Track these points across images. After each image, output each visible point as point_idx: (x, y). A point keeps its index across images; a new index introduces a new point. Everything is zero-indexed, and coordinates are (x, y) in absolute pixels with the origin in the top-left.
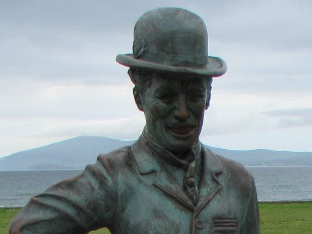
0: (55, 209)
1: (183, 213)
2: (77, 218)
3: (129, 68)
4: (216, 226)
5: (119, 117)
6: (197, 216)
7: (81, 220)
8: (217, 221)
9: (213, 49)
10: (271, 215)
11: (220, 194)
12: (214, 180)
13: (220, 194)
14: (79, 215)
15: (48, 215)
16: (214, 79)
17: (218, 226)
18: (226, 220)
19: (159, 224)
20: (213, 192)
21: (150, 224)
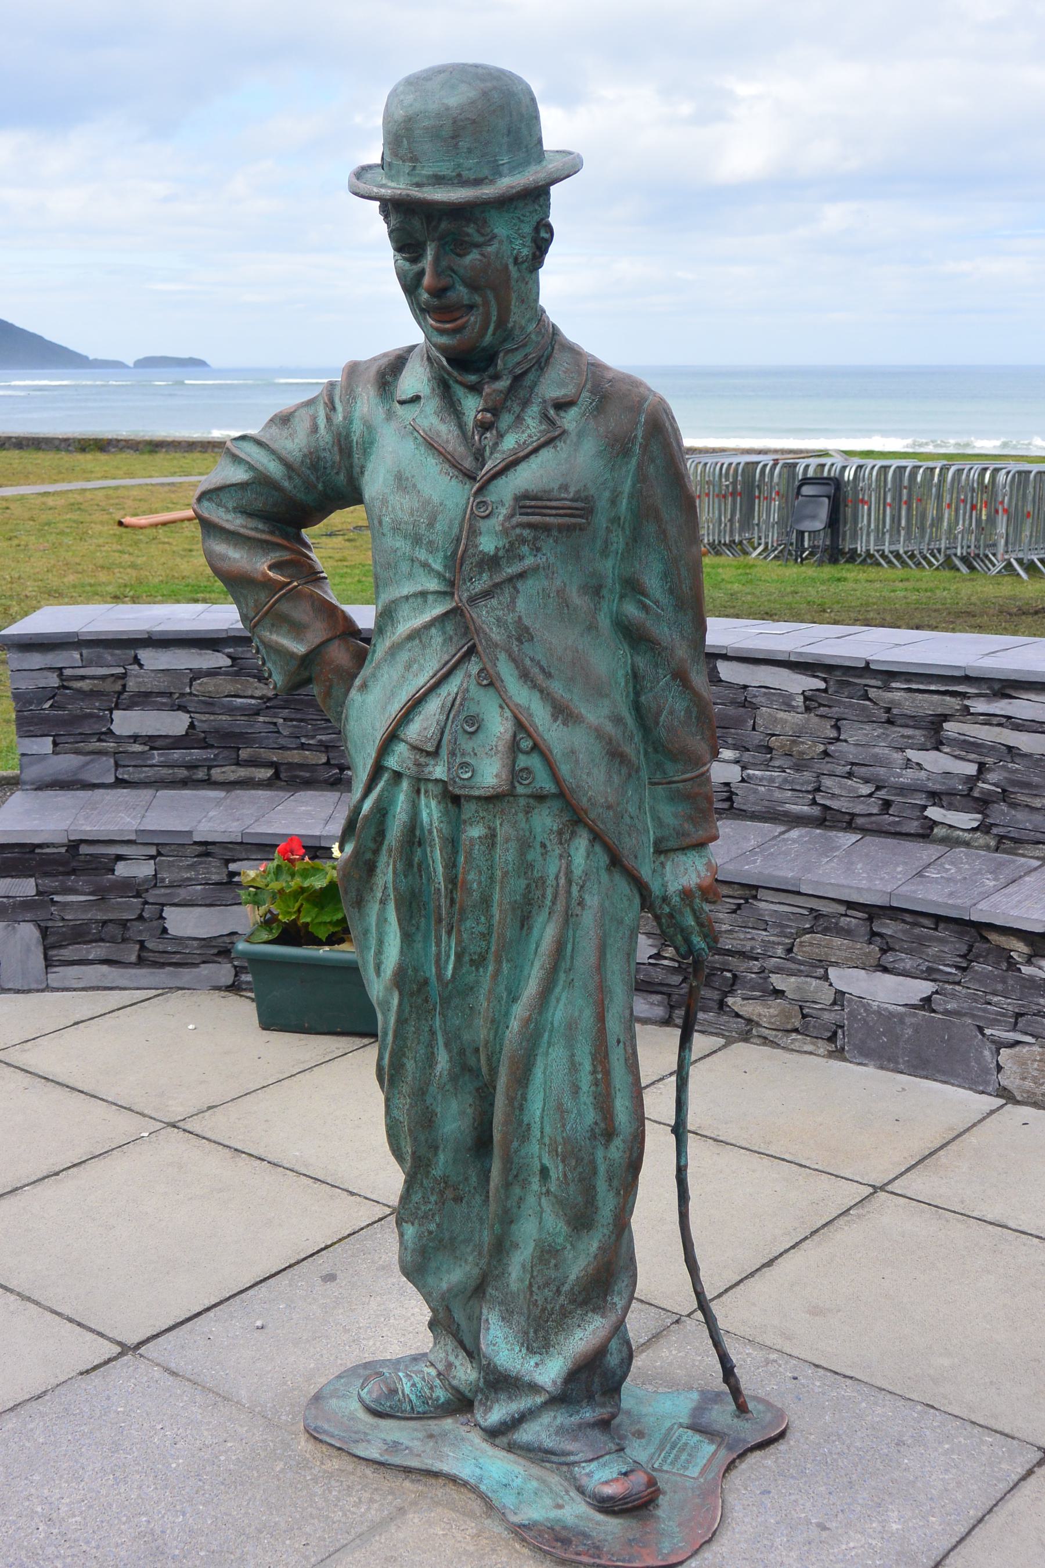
0: (251, 467)
1: (454, 482)
2: (286, 484)
3: (378, 203)
4: (521, 514)
5: (369, 308)
6: (480, 490)
7: (295, 487)
8: (528, 503)
9: (556, 130)
10: (763, 970)
11: (555, 447)
12: (545, 417)
13: (555, 447)
14: (290, 478)
15: (239, 475)
16: (553, 189)
17: (527, 514)
18: (549, 503)
19: (401, 504)
20: (533, 442)
21: (387, 502)
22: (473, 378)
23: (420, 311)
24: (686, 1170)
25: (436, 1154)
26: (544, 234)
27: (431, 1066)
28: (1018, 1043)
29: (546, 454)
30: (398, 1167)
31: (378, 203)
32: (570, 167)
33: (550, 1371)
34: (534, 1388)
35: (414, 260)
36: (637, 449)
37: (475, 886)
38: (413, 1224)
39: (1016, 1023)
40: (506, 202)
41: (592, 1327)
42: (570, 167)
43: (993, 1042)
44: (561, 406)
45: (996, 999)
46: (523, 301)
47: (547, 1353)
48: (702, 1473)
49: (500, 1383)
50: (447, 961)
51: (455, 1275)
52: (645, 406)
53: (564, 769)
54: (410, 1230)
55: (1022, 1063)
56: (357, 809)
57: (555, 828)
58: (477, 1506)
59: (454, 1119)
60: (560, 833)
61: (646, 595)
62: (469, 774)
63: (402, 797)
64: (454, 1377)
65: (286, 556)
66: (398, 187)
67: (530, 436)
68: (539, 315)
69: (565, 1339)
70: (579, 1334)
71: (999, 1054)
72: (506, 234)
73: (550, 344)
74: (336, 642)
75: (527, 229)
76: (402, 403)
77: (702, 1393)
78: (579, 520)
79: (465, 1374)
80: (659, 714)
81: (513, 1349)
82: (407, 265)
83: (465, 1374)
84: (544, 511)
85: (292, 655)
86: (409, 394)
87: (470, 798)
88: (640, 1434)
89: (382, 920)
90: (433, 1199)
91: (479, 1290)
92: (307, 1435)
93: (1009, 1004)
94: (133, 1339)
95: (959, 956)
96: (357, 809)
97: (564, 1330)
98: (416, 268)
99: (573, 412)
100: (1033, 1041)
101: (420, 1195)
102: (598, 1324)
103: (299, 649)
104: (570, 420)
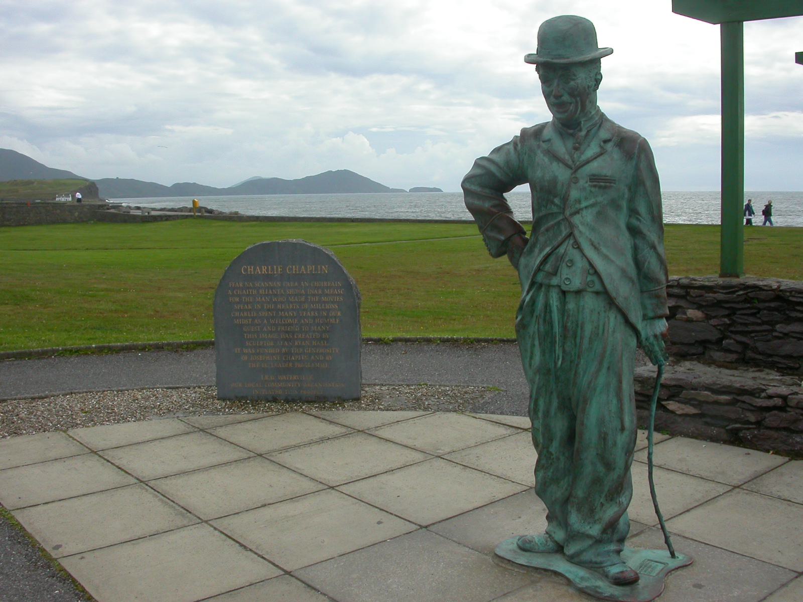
22: (571, 131)
23: (551, 105)
24: (652, 454)
25: (552, 443)
26: (599, 77)
29: (600, 160)
30: (535, 450)
31: (534, 66)
32: (609, 52)
33: (595, 530)
34: (589, 537)
35: (549, 86)
36: (635, 157)
40: (583, 64)
42: (609, 52)
44: (605, 142)
46: (590, 102)
48: (656, 575)
49: (573, 536)
50: (558, 359)
51: (558, 492)
52: (639, 141)
53: (607, 282)
54: (541, 474)
56: (524, 301)
58: (563, 581)
59: (559, 426)
61: (640, 215)
62: (570, 265)
65: (497, 202)
66: (541, 60)
68: (598, 110)
72: (581, 78)
73: (603, 118)
74: (516, 236)
75: (592, 75)
76: (544, 142)
77: (647, 438)
79: (560, 535)
80: (644, 263)
83: (560, 535)
85: (499, 240)
86: (547, 138)
87: (569, 292)
88: (617, 214)
89: (533, 345)
91: (566, 501)
94: (424, 524)
96: (524, 301)
103: (503, 238)
104: (609, 146)
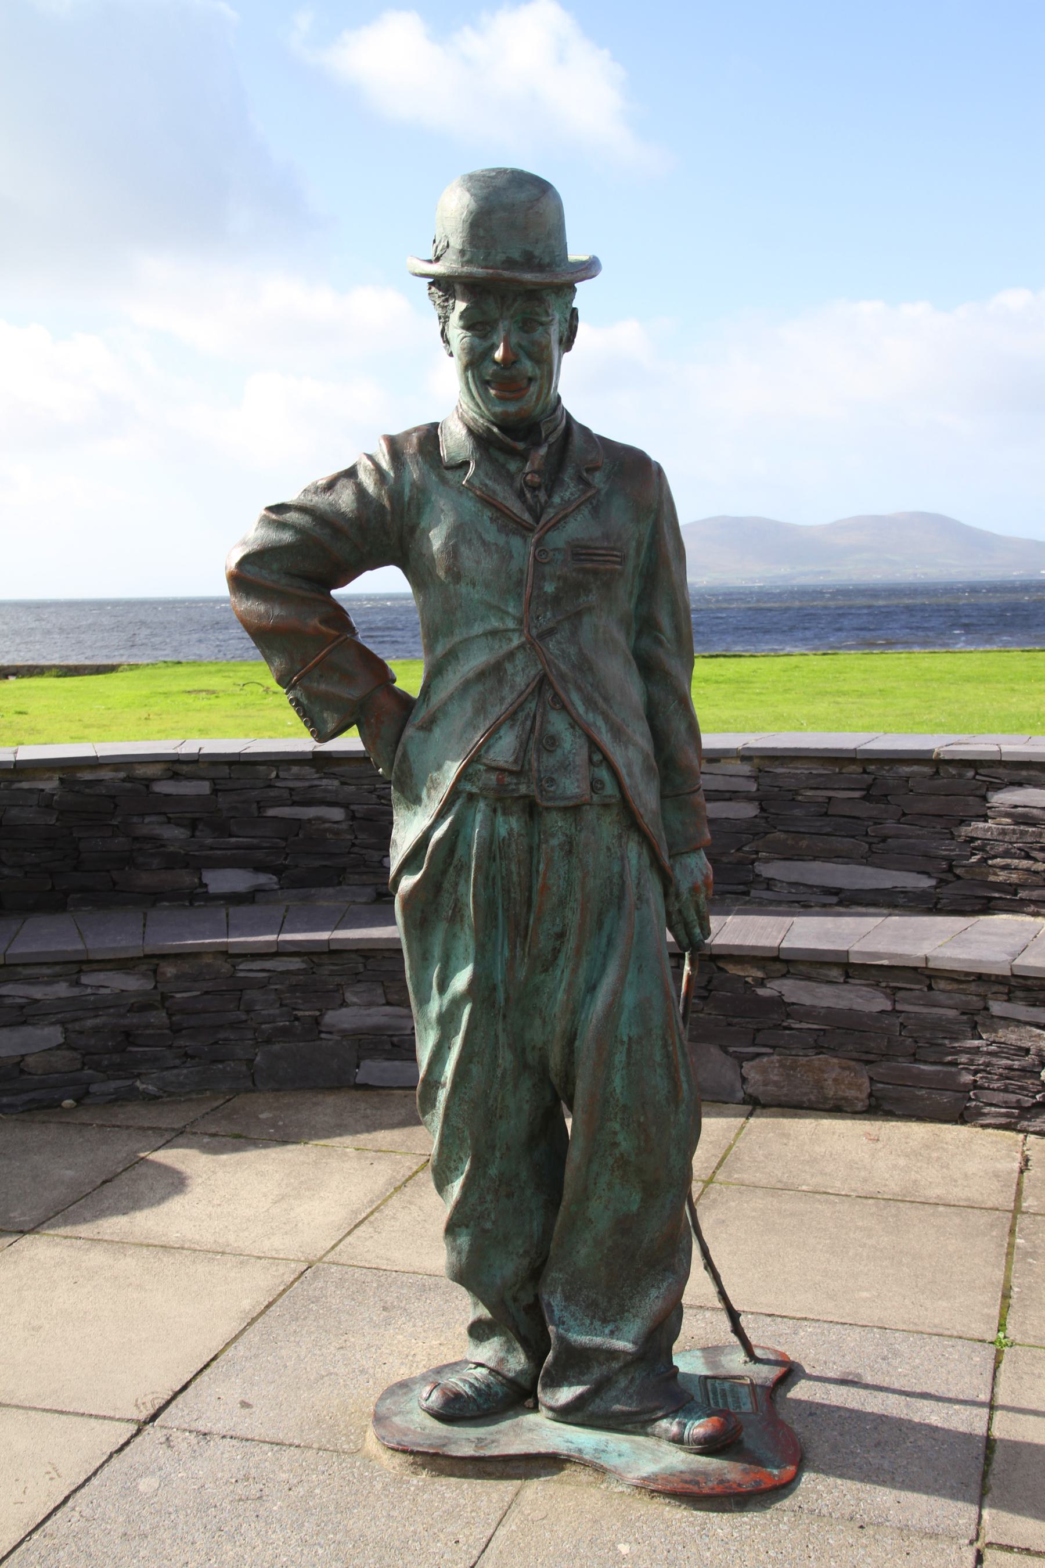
12: (580, 479)
18: (597, 552)
27: (494, 1069)
28: (758, 1055)
37: (555, 889)
38: (467, 1227)
39: (754, 1039)
41: (665, 1284)
42: (589, 269)
43: (736, 1057)
45: (736, 1020)
47: (621, 1318)
55: (764, 1071)
57: (616, 833)
60: (620, 837)
63: (479, 817)
64: (509, 1371)
67: (572, 494)
69: (640, 1301)
70: (654, 1293)
71: (742, 1067)
76: (448, 468)
78: (617, 567)
81: (583, 1324)
82: (477, 341)
84: (595, 558)
90: (489, 1198)
92: (391, 1452)
93: (748, 1022)
95: (701, 988)
97: (638, 1292)
98: (486, 344)
99: (598, 474)
100: (771, 1051)
101: (477, 1196)
102: (670, 1280)
